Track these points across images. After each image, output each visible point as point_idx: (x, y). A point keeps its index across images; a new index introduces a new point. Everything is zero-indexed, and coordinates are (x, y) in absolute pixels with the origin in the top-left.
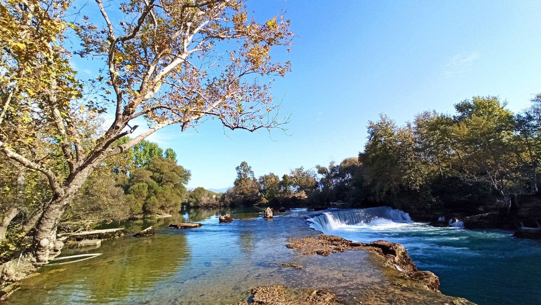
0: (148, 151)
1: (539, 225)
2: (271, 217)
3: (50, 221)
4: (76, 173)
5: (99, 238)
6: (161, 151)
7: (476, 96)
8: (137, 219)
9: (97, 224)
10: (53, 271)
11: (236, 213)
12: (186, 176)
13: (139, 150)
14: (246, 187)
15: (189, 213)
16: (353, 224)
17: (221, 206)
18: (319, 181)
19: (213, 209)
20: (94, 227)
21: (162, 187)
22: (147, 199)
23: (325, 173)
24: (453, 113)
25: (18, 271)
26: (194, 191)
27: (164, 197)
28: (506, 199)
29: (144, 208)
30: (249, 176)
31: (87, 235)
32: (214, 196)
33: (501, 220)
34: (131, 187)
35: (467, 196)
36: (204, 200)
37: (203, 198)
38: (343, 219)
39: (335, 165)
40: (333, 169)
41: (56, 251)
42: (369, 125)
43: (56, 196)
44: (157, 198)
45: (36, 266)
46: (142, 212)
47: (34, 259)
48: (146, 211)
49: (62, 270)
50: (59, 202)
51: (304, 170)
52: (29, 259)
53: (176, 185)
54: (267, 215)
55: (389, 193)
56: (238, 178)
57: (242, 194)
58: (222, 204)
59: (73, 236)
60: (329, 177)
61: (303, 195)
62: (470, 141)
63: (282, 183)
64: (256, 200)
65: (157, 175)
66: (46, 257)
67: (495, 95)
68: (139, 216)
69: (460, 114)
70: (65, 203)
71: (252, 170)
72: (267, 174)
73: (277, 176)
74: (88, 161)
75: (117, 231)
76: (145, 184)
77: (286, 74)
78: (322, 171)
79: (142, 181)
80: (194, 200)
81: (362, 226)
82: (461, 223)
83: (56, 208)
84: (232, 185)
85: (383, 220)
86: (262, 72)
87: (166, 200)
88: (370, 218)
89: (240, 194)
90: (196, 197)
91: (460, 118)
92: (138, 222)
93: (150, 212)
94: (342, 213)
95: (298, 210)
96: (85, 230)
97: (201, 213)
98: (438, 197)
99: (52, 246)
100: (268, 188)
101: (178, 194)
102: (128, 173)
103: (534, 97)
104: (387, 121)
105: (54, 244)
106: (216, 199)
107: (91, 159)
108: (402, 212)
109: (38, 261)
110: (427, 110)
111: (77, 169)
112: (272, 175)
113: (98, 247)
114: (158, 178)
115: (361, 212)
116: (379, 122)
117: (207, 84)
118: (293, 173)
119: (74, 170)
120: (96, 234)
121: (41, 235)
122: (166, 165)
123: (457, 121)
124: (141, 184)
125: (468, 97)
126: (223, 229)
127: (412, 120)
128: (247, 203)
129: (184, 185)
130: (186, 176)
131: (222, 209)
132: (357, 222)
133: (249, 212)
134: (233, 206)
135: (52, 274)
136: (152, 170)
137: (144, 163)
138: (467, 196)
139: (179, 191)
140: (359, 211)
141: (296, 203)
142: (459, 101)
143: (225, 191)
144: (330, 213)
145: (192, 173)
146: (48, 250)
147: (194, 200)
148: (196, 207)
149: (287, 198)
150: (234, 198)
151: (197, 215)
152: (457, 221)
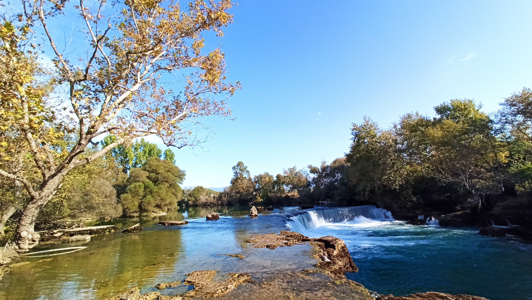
0: (148, 151)
1: (509, 224)
2: (256, 216)
3: (28, 217)
4: (48, 180)
5: (90, 234)
6: (159, 152)
7: (454, 99)
8: (134, 217)
9: (97, 221)
10: (41, 261)
11: (232, 211)
12: (181, 176)
13: (139, 150)
14: (241, 186)
15: (188, 212)
16: (337, 222)
17: (218, 205)
18: (310, 180)
19: (211, 207)
20: (94, 224)
21: (157, 186)
22: (143, 199)
23: (317, 173)
24: (432, 115)
25: (5, 256)
26: (193, 191)
27: (160, 196)
28: (476, 198)
29: (140, 206)
30: (245, 175)
31: (79, 231)
32: (212, 195)
33: (476, 218)
34: (129, 187)
35: (446, 195)
36: (203, 198)
37: (201, 197)
38: (326, 217)
39: (326, 164)
40: (324, 169)
41: (34, 241)
42: (352, 127)
43: (33, 198)
44: (152, 197)
45: (18, 253)
46: (138, 210)
47: (17, 247)
48: (142, 209)
49: (49, 260)
50: (35, 203)
51: (297, 170)
52: (13, 247)
53: (171, 185)
54: (252, 213)
55: (372, 192)
56: (234, 177)
58: (220, 202)
59: (67, 232)
60: (320, 177)
61: (295, 194)
62: (442, 144)
64: (251, 199)
65: (153, 175)
66: (26, 246)
67: (471, 98)
68: (135, 215)
69: (438, 117)
70: (40, 204)
71: (248, 169)
72: (262, 173)
73: (272, 176)
74: (59, 171)
75: (108, 228)
76: (141, 184)
77: (235, 93)
78: (313, 171)
79: (139, 181)
80: (193, 199)
81: (346, 224)
82: (437, 221)
83: (33, 207)
84: (229, 185)
85: (362, 218)
86: (215, 91)
87: (162, 199)
88: (353, 217)
89: (236, 193)
90: (195, 195)
91: (440, 120)
92: (135, 219)
93: (146, 211)
94: (326, 211)
95: (291, 208)
96: (79, 227)
97: (200, 212)
98: (419, 196)
99: (30, 237)
100: (263, 187)
101: (173, 193)
102: (128, 172)
103: (503, 101)
104: (370, 123)
105: (32, 235)
106: (214, 198)
107: (61, 169)
108: (385, 210)
109: (20, 248)
110: (409, 112)
111: (49, 177)
112: (267, 174)
113: (87, 241)
114: (154, 178)
115: (345, 210)
116: (363, 124)
117: (173, 100)
118: (286, 172)
119: (47, 178)
120: (87, 230)
121: (22, 228)
122: (162, 165)
123: (436, 122)
124: (138, 184)
125: (446, 100)
126: (209, 226)
127: (398, 121)
128: (251, 201)
129: (179, 184)
130: (181, 176)
131: (220, 208)
132: (341, 221)
133: (245, 210)
134: (229, 204)
135: (40, 263)
136: (148, 171)
137: (143, 162)
138: (446, 195)
139: (174, 190)
140: (343, 209)
141: (289, 201)
142: (439, 103)
143: (222, 191)
144: (315, 211)
145: (186, 173)
146: (27, 240)
147: (193, 199)
148: (195, 206)
149: (281, 197)
150: (231, 197)
151: (196, 213)
152: (433, 219)
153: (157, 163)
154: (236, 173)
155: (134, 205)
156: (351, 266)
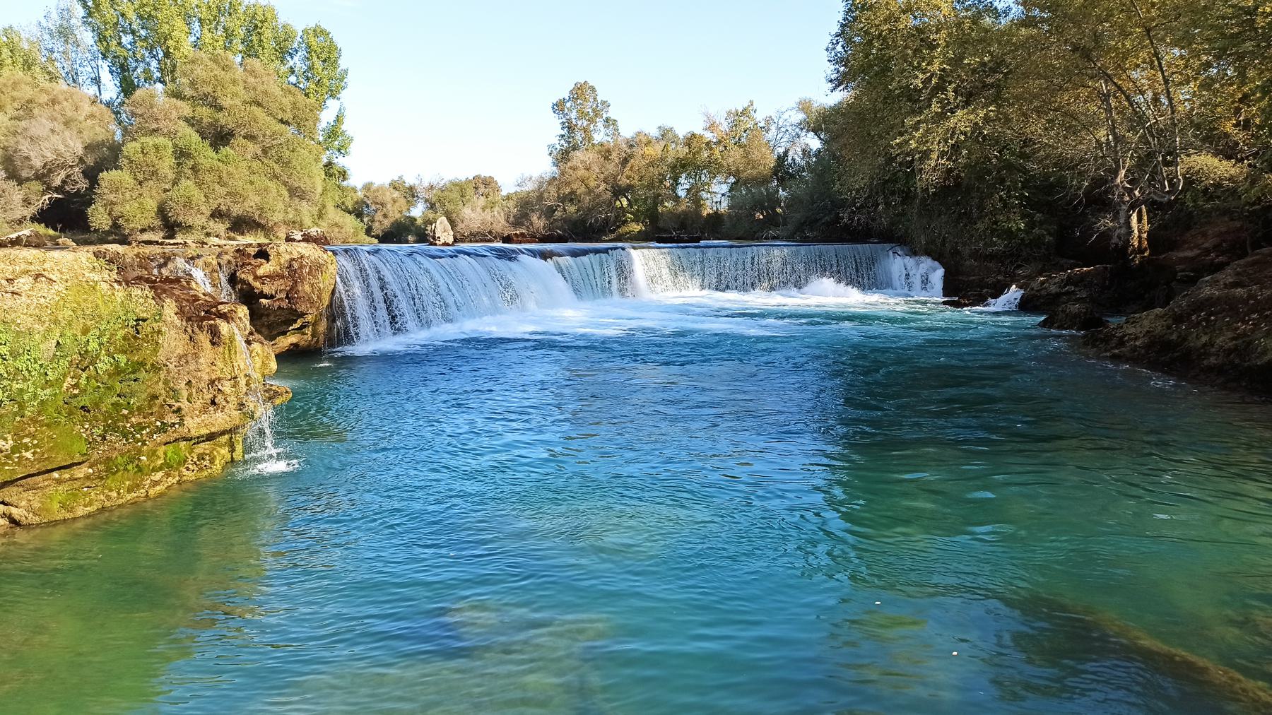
27: (221, 182)
29: (162, 211)
44: (199, 184)
46: (157, 222)
51: (760, 117)
57: (572, 198)
63: (681, 166)
65: (204, 113)
71: (612, 113)
84: (544, 167)
87: (229, 193)
89: (563, 199)
90: (449, 207)
112: (666, 134)
118: (712, 127)
122: (234, 82)
124: (150, 141)
154: (570, 127)
155: (142, 208)
156: (287, 297)
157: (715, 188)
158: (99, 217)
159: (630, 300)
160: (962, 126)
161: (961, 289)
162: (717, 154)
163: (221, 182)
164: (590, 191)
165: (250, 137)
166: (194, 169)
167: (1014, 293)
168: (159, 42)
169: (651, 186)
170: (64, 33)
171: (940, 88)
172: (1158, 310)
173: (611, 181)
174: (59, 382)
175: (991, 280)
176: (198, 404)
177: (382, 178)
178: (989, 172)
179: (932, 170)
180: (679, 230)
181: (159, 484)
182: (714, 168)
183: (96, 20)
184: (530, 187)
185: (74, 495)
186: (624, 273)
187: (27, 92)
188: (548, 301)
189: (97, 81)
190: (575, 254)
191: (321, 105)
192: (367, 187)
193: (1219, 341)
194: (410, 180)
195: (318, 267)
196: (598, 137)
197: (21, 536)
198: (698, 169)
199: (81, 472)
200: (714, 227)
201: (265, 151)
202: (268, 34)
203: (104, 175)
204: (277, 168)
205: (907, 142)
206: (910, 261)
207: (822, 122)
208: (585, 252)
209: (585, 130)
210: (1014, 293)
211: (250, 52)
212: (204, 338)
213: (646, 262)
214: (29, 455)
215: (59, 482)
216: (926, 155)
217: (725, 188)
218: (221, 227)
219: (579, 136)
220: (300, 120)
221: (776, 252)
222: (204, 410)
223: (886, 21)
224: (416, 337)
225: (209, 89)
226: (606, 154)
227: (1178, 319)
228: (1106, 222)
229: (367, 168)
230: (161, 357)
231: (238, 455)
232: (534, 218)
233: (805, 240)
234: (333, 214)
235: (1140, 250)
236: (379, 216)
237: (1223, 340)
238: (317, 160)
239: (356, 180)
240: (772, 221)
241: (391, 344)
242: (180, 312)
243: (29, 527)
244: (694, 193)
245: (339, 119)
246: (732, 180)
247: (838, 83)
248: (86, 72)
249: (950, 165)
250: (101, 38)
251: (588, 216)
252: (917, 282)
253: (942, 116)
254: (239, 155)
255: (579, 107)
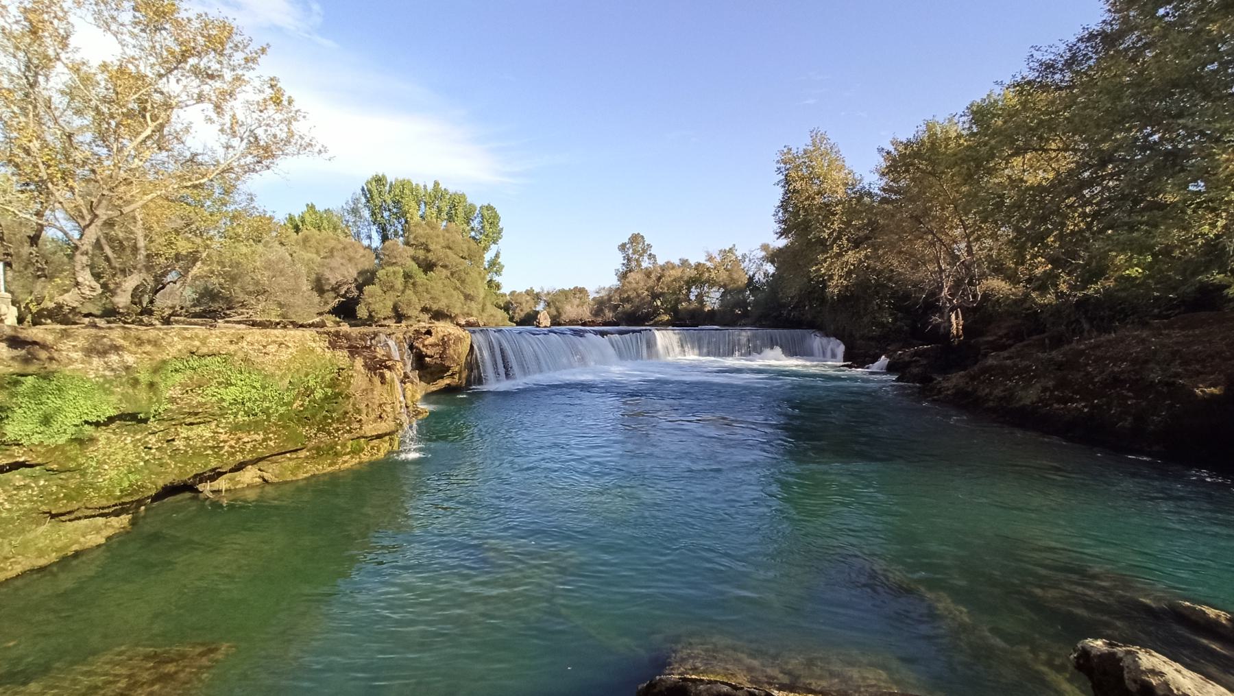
27: (427, 291)
29: (395, 308)
44: (416, 293)
51: (739, 253)
57: (628, 300)
63: (691, 282)
65: (421, 254)
71: (653, 251)
84: (612, 281)
89: (623, 300)
112: (684, 263)
118: (710, 259)
122: (438, 236)
124: (391, 269)
153: (428, 230)
157: (712, 295)
158: (362, 312)
159: (654, 361)
160: (851, 260)
161: (854, 357)
162: (713, 275)
163: (427, 291)
164: (638, 295)
165: (445, 267)
166: (414, 284)
167: (884, 360)
168: (402, 214)
169: (674, 293)
170: (355, 211)
171: (839, 238)
172: (962, 373)
173: (650, 289)
174: (290, 404)
175: (871, 353)
176: (373, 417)
177: (521, 288)
178: (869, 288)
179: (834, 288)
180: (688, 320)
181: (348, 462)
182: (712, 283)
183: (371, 205)
184: (603, 294)
185: (298, 467)
186: (651, 344)
187: (333, 243)
188: (607, 362)
189: (370, 237)
190: (621, 333)
191: (486, 249)
192: (512, 293)
193: (996, 392)
194: (537, 290)
195: (459, 340)
196: (645, 264)
197: (268, 488)
198: (703, 283)
199: (302, 454)
200: (711, 318)
201: (452, 274)
202: (460, 209)
203: (366, 288)
204: (458, 284)
205: (819, 270)
206: (825, 340)
207: (775, 256)
208: (627, 332)
209: (637, 260)
210: (884, 360)
211: (450, 219)
212: (377, 380)
213: (665, 339)
214: (272, 443)
215: (290, 459)
216: (831, 277)
217: (718, 295)
218: (426, 317)
219: (633, 264)
220: (473, 257)
221: (744, 333)
222: (375, 421)
223: (807, 199)
224: (519, 382)
225: (423, 240)
226: (648, 274)
227: (973, 378)
228: (936, 319)
229: (511, 282)
230: (351, 390)
231: (396, 448)
232: (607, 311)
233: (762, 326)
234: (491, 309)
235: (958, 336)
236: (518, 310)
237: (998, 392)
238: (484, 278)
239: (506, 289)
240: (746, 314)
241: (505, 385)
242: (365, 365)
243: (272, 484)
244: (700, 297)
245: (497, 256)
246: (722, 290)
247: (783, 233)
248: (364, 232)
249: (845, 283)
250: (373, 214)
251: (633, 312)
252: (829, 353)
253: (839, 255)
254: (439, 274)
255: (635, 246)
